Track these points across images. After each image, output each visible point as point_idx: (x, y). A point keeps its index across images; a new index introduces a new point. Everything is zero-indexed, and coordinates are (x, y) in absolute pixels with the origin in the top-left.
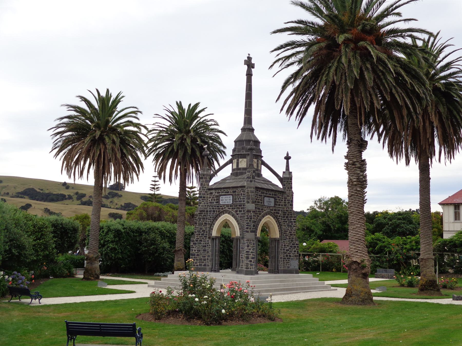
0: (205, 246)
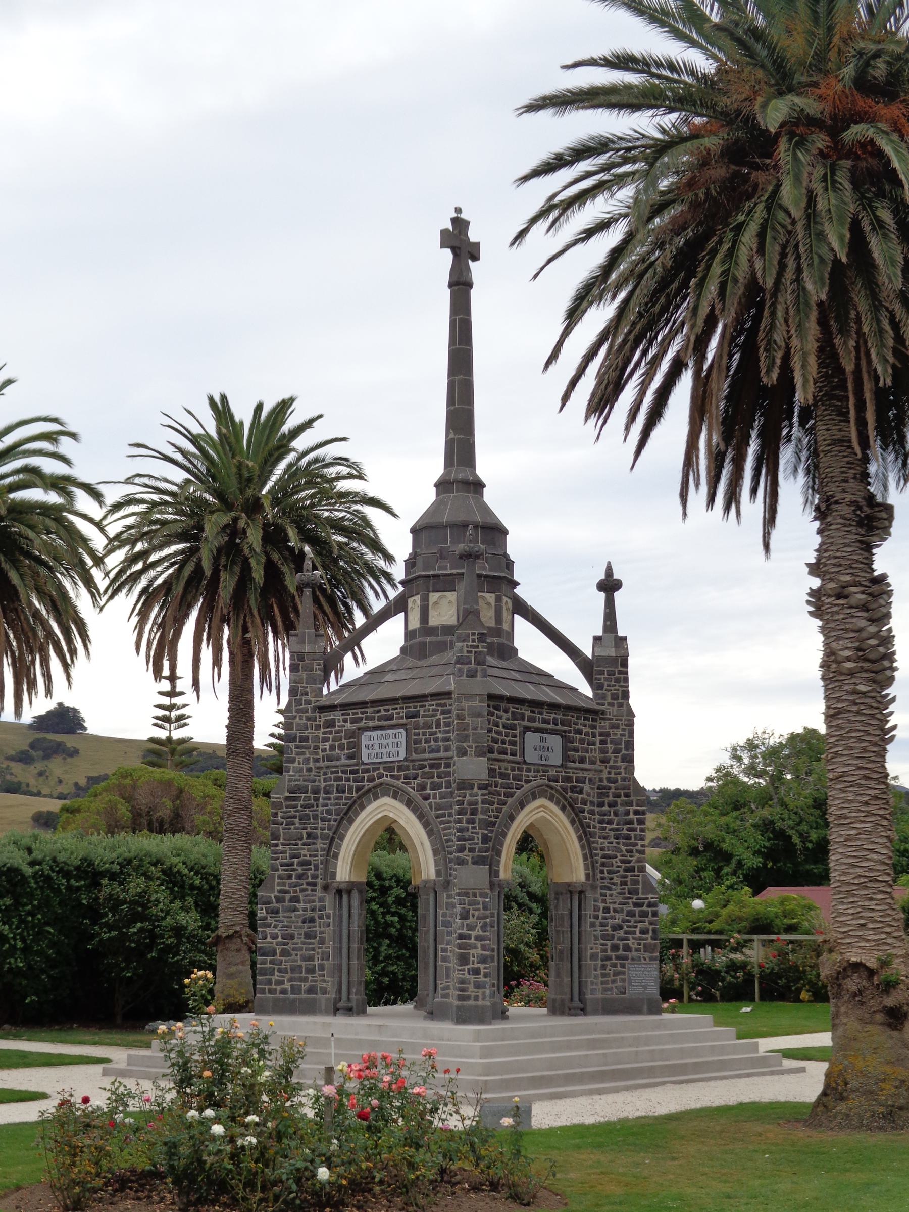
0: (312, 920)
